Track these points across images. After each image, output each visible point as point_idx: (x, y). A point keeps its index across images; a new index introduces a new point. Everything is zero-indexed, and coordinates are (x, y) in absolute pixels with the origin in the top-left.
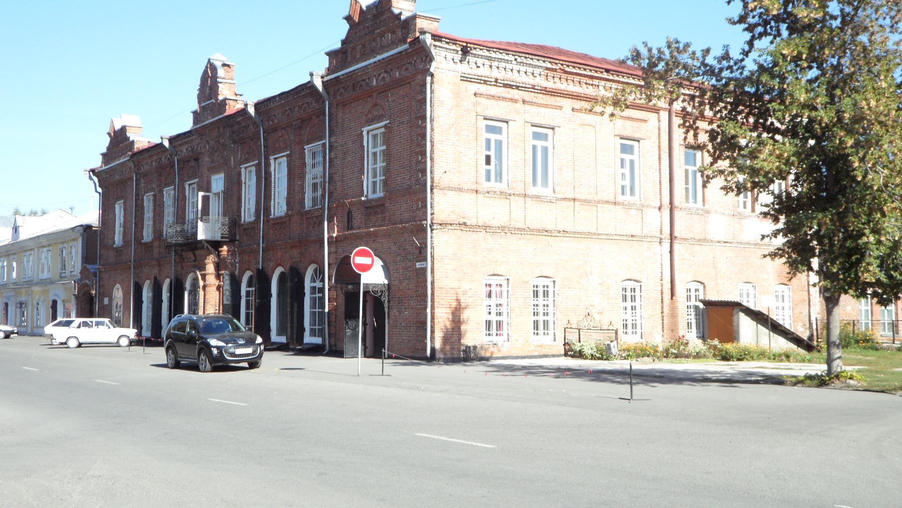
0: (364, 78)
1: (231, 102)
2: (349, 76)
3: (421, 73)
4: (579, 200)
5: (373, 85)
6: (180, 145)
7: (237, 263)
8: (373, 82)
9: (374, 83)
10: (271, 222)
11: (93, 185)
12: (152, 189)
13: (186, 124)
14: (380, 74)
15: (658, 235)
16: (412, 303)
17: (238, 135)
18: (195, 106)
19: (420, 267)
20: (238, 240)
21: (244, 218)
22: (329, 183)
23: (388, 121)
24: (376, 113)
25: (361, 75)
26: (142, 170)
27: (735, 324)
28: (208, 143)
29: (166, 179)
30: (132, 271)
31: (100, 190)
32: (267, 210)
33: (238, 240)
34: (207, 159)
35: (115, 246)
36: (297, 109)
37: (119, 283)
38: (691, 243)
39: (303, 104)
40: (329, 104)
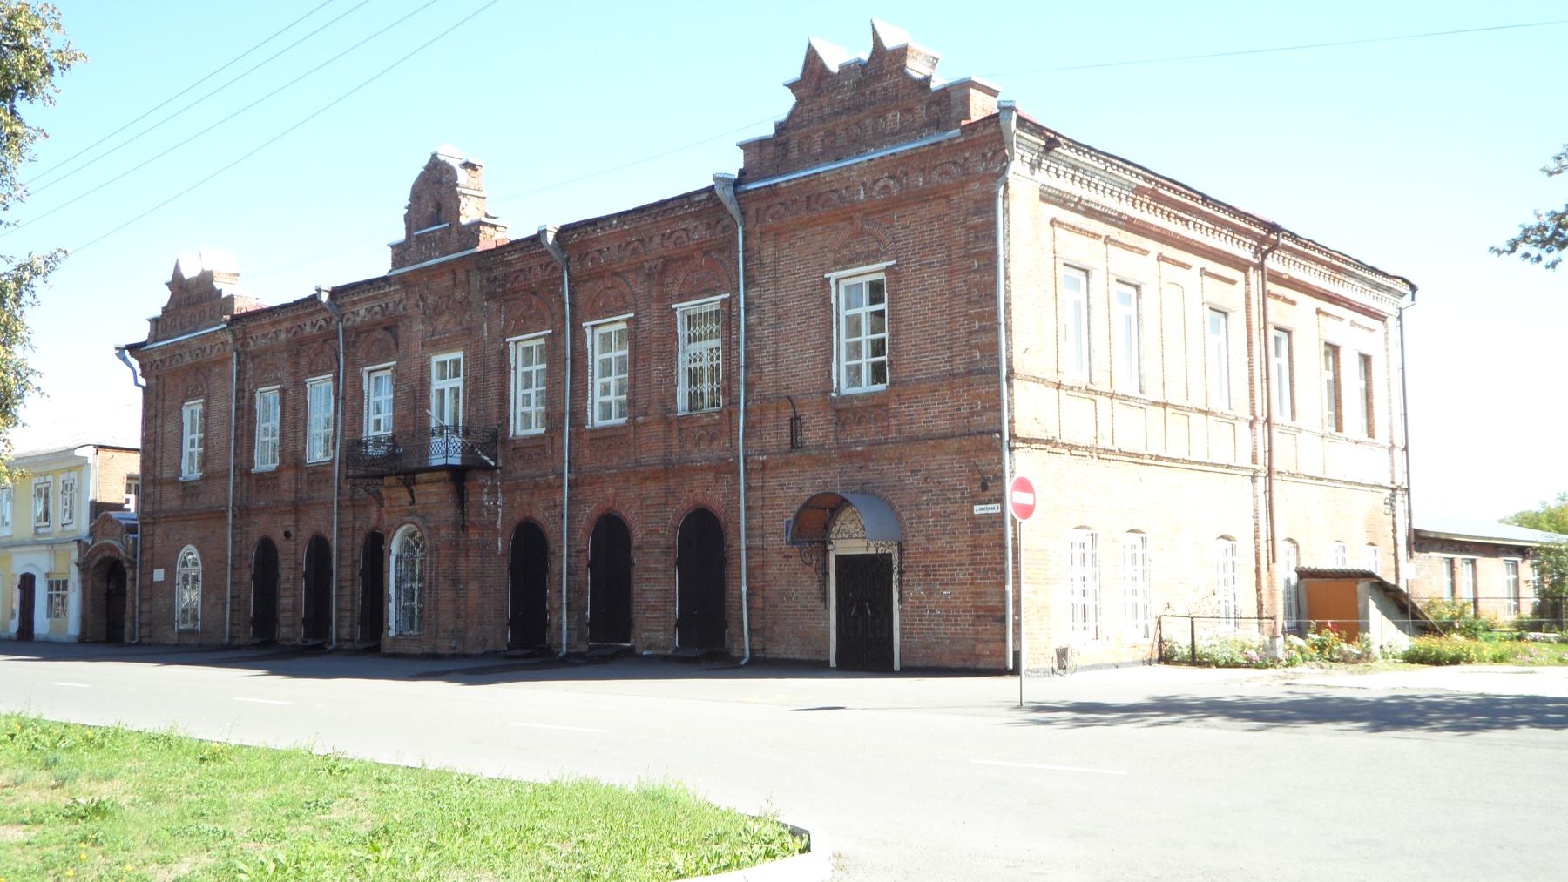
0: (836, 186)
1: (487, 229)
2: (801, 183)
3: (978, 180)
4: (1174, 406)
5: (858, 199)
6: (354, 303)
7: (500, 506)
8: (859, 194)
9: (862, 196)
10: (586, 437)
11: (131, 372)
12: (276, 381)
13: (379, 265)
14: (875, 182)
15: (1248, 463)
16: (962, 576)
17: (503, 286)
18: (400, 235)
19: (978, 512)
20: (500, 468)
21: (515, 429)
22: (746, 368)
23: (894, 262)
24: (859, 248)
25: (830, 182)
26: (252, 347)
27: (385, 618)
28: (423, 299)
29: (311, 363)
30: (230, 522)
31: (142, 382)
32: (578, 414)
33: (500, 468)
34: (418, 327)
35: (181, 478)
36: (657, 240)
37: (193, 544)
38: (1284, 478)
39: (673, 233)
40: (744, 231)
